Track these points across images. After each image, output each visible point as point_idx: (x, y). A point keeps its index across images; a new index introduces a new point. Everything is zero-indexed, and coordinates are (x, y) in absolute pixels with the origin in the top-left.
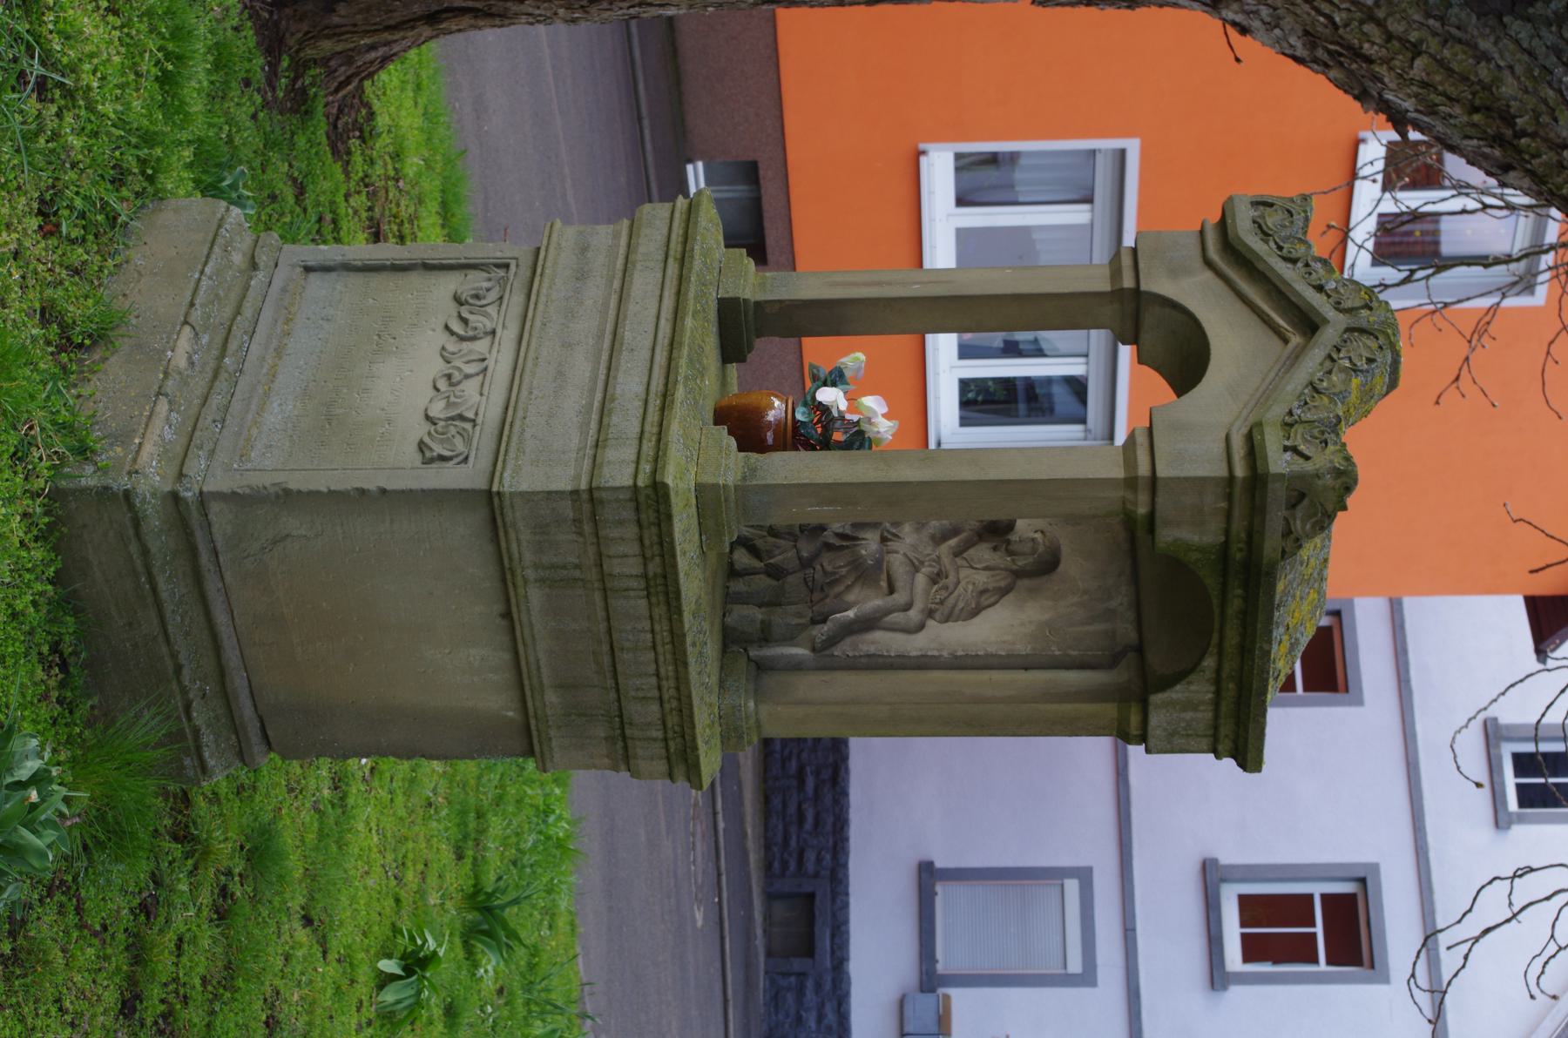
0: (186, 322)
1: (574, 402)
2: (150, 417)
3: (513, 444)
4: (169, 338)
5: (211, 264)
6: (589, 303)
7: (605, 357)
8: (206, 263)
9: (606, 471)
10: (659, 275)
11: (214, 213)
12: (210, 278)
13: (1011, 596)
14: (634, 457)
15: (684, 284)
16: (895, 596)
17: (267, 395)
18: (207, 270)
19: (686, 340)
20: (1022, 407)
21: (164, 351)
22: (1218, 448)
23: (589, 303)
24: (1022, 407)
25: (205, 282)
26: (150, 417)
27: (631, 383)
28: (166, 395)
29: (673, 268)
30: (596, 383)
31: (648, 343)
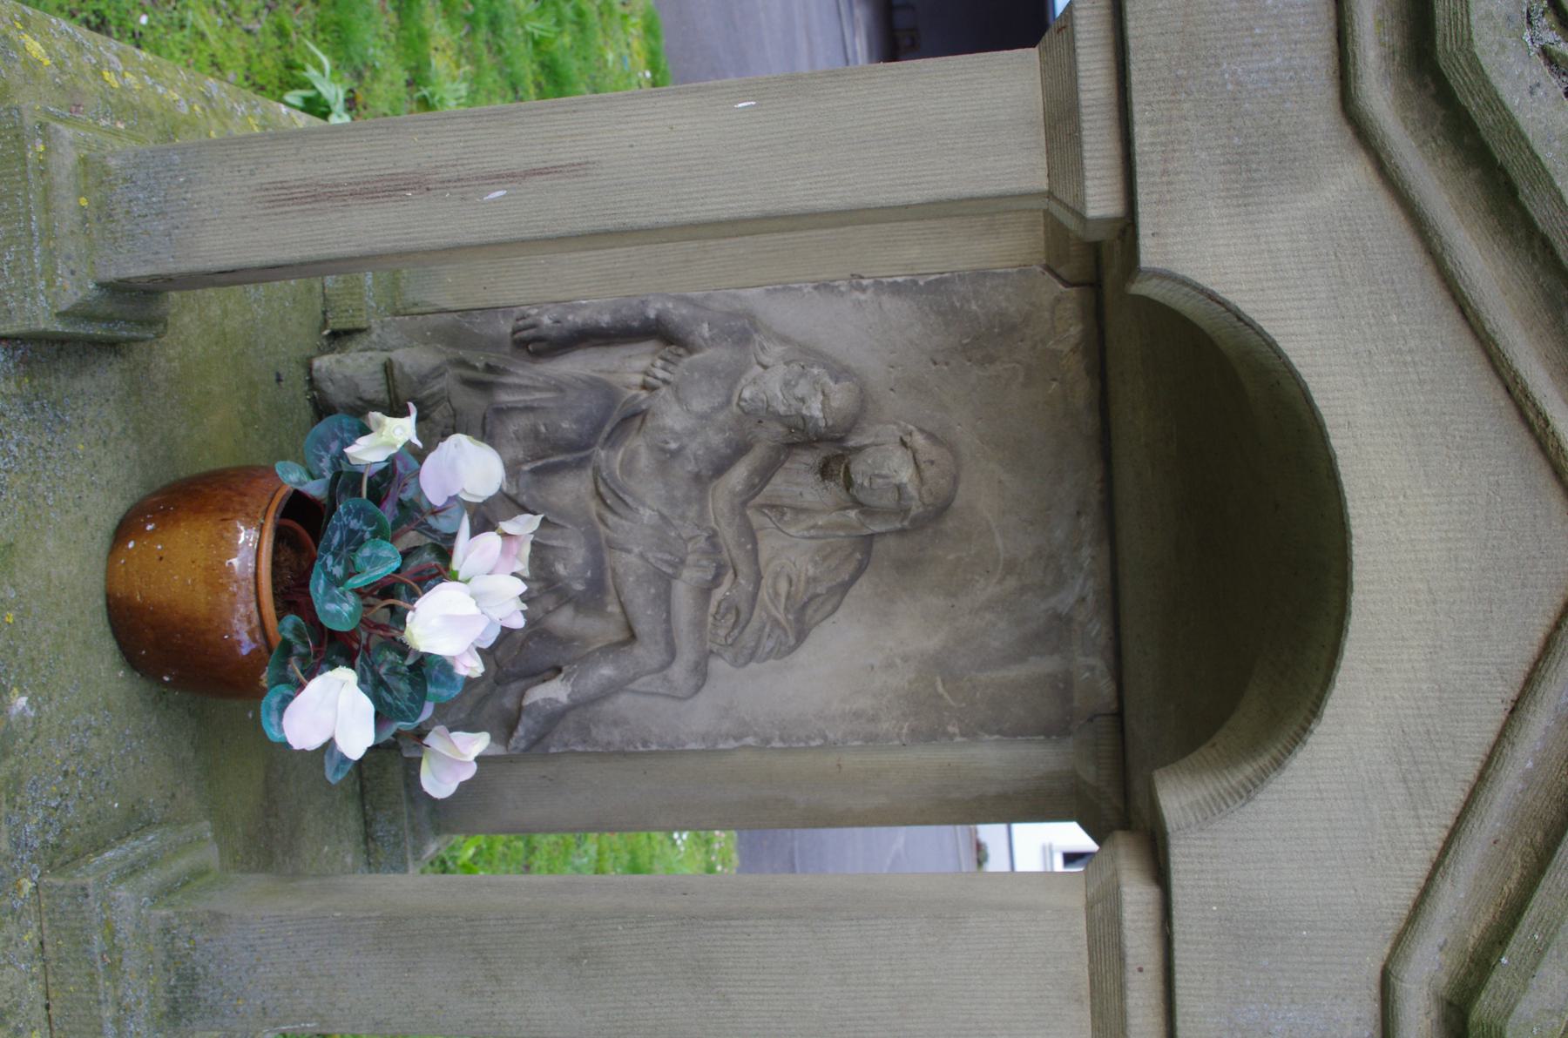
13: (863, 586)
16: (638, 651)
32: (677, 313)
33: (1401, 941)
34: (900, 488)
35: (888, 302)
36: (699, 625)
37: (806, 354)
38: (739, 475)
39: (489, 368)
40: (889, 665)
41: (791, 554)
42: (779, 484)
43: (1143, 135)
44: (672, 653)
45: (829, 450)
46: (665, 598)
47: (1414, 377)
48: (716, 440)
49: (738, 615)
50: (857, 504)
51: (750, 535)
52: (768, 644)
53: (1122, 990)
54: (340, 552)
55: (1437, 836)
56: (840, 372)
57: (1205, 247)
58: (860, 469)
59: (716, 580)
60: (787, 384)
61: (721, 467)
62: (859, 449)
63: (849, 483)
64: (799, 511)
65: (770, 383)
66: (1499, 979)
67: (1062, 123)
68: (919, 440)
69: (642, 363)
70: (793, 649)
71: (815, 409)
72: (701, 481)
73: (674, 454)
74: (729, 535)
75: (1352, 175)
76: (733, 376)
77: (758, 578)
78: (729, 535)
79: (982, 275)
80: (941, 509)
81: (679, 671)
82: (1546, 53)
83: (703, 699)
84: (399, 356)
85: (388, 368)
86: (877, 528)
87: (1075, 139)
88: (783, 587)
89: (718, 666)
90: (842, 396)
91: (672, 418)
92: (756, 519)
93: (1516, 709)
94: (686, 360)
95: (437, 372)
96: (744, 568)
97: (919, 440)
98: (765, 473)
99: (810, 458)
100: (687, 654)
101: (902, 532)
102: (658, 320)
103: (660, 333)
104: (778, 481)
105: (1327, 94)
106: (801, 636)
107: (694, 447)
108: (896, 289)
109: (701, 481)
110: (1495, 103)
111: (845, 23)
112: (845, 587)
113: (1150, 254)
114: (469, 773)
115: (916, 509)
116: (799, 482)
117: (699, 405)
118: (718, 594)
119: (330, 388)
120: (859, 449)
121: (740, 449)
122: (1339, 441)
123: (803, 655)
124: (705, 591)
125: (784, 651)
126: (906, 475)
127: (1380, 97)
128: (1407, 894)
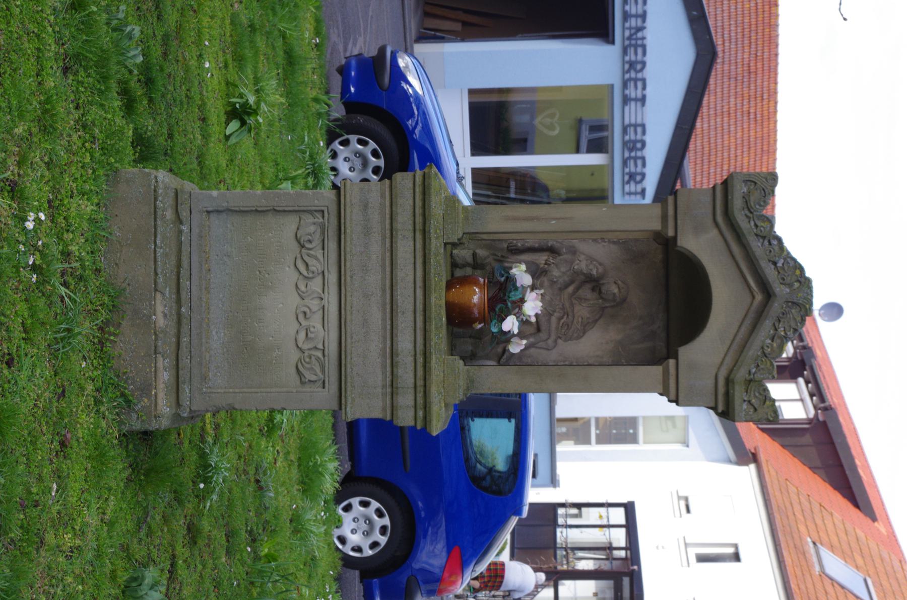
0: (156, 290)
1: (375, 346)
2: (156, 371)
3: (349, 384)
4: (150, 304)
5: (159, 237)
6: (374, 257)
7: (388, 307)
8: (155, 237)
9: (400, 413)
10: (412, 243)
11: (149, 186)
12: (161, 247)
13: (601, 322)
14: (412, 403)
15: (427, 264)
16: (541, 334)
17: (208, 325)
18: (158, 242)
19: (433, 316)
20: (605, 134)
21: (151, 317)
22: (710, 382)
23: (374, 257)
24: (605, 134)
25: (160, 252)
26: (156, 371)
27: (405, 343)
28: (160, 353)
29: (419, 236)
30: (385, 331)
31: (411, 308)
32: (557, 245)
33: (719, 369)
34: (614, 294)
35: (612, 246)
36: (557, 328)
37: (591, 259)
38: (571, 289)
39: (502, 256)
40: (607, 343)
41: (582, 311)
42: (581, 292)
43: (679, 222)
44: (550, 336)
45: (594, 283)
46: (549, 321)
47: (74, 88)
48: (567, 279)
49: (568, 326)
50: (602, 298)
51: (572, 305)
52: (575, 335)
53: (669, 379)
54: (503, 297)
55: (725, 350)
56: (600, 264)
57: (689, 242)
58: (604, 289)
59: (562, 318)
60: (587, 266)
61: (567, 286)
62: (603, 284)
63: (600, 292)
64: (586, 300)
65: (582, 265)
66: (734, 372)
67: (664, 218)
68: (619, 282)
69: (545, 258)
70: (581, 337)
71: (594, 272)
72: (561, 289)
73: (555, 282)
74: (567, 305)
75: (715, 232)
76: (572, 262)
77: (574, 317)
78: (567, 305)
79: (636, 240)
80: (624, 300)
81: (550, 342)
82: (746, 215)
83: (554, 351)
84: (478, 251)
85: (474, 255)
86: (607, 305)
87: (667, 221)
88: (580, 319)
89: (560, 341)
90: (601, 270)
91: (556, 273)
92: (574, 301)
93: (740, 327)
94: (559, 258)
95: (488, 257)
96: (570, 314)
97: (619, 282)
98: (577, 289)
99: (589, 286)
100: (553, 337)
101: (612, 307)
102: (551, 247)
103: (552, 251)
104: (580, 291)
105: (710, 217)
106: (584, 333)
107: (561, 280)
108: (614, 243)
109: (561, 289)
110: (737, 223)
111: (743, 329)
112: (596, 321)
113: (679, 243)
114: (523, 347)
115: (618, 300)
116: (586, 292)
117: (563, 269)
118: (562, 321)
119: (457, 259)
120: (603, 284)
121: (572, 282)
122: (711, 279)
123: (583, 340)
124: (560, 319)
125: (579, 338)
126: (616, 291)
127: (720, 219)
128: (720, 360)
